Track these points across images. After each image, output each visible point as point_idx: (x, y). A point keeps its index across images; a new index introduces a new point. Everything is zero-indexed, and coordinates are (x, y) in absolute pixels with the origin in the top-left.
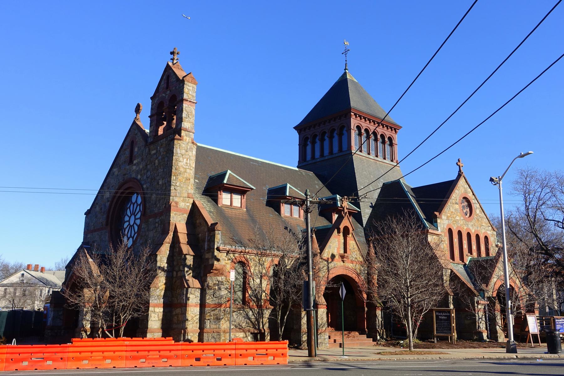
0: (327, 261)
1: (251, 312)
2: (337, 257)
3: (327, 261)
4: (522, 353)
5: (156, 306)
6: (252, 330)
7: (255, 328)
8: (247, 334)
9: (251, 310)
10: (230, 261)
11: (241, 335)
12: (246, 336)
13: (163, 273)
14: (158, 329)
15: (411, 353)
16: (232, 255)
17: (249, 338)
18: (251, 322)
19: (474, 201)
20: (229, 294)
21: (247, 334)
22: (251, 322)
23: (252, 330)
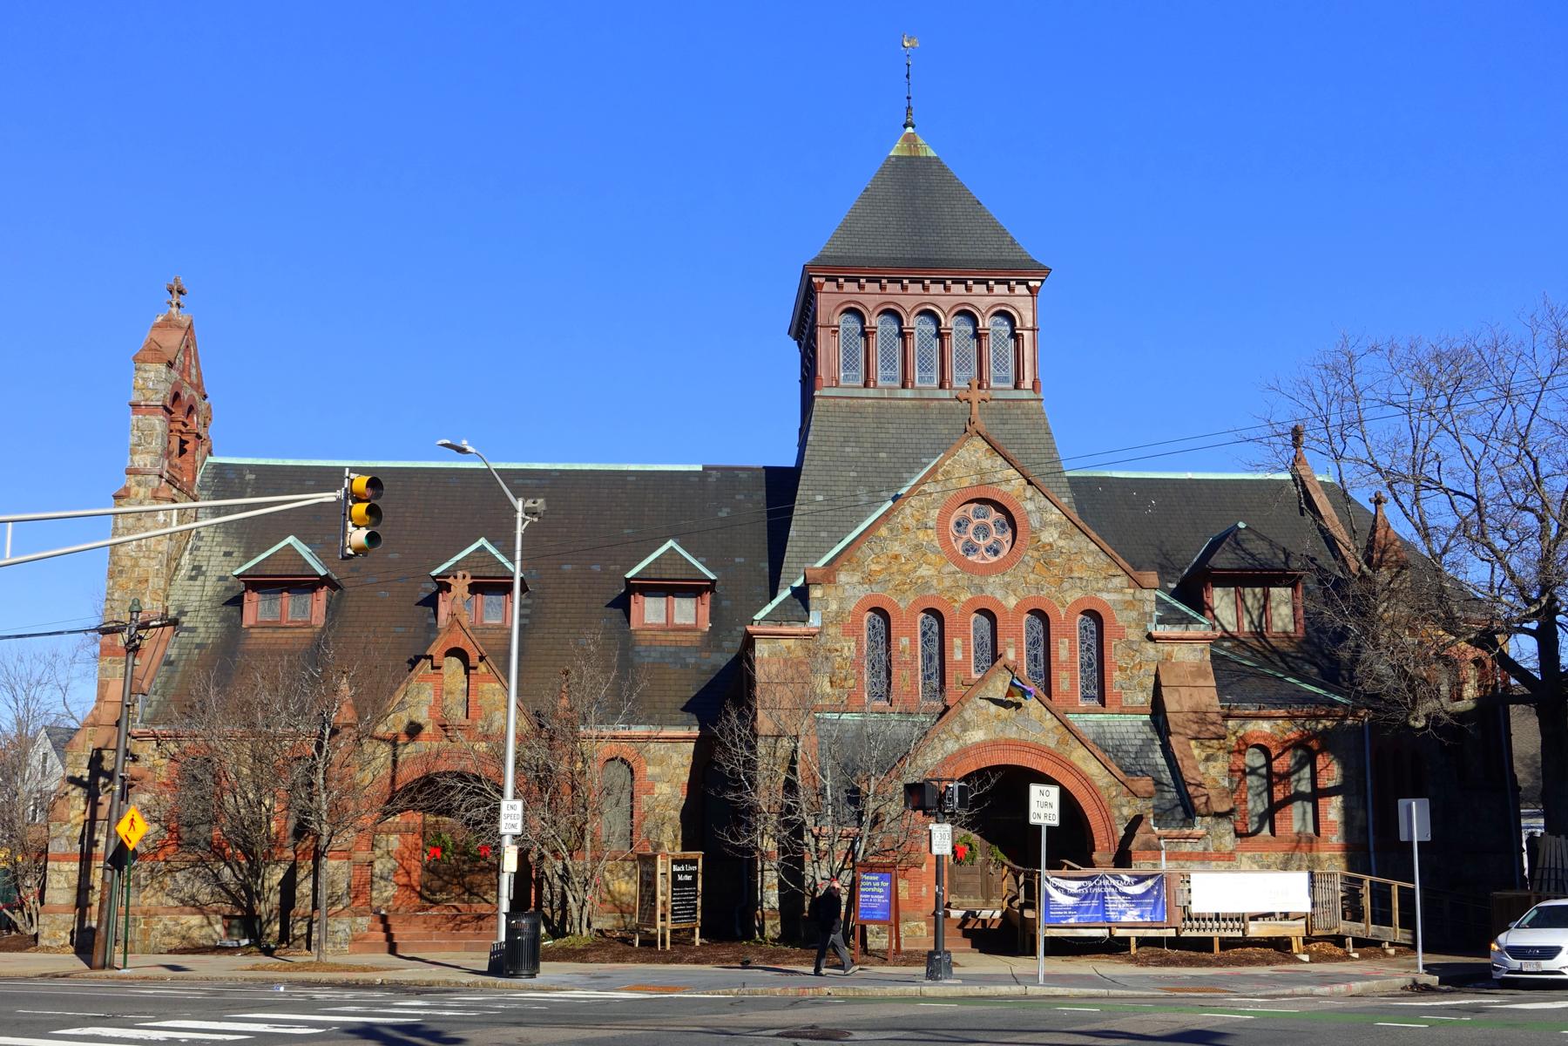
0: (394, 742)
1: (227, 871)
2: (429, 729)
3: (394, 742)
4: (558, 982)
5: (64, 858)
6: (227, 909)
7: (240, 906)
8: (213, 917)
9: (227, 864)
10: (165, 761)
11: (196, 920)
12: (210, 924)
13: (79, 790)
14: (67, 905)
15: (1217, 963)
16: (172, 747)
17: (219, 928)
18: (228, 892)
19: (1030, 506)
20: (163, 832)
21: (213, 917)
22: (228, 892)
23: (227, 909)
